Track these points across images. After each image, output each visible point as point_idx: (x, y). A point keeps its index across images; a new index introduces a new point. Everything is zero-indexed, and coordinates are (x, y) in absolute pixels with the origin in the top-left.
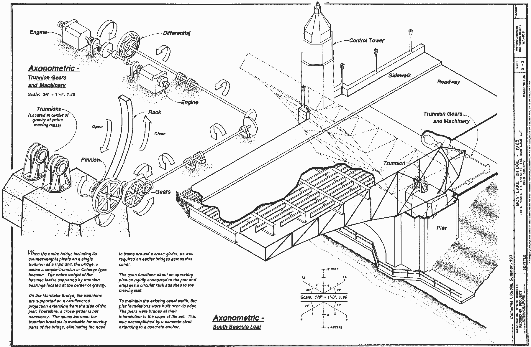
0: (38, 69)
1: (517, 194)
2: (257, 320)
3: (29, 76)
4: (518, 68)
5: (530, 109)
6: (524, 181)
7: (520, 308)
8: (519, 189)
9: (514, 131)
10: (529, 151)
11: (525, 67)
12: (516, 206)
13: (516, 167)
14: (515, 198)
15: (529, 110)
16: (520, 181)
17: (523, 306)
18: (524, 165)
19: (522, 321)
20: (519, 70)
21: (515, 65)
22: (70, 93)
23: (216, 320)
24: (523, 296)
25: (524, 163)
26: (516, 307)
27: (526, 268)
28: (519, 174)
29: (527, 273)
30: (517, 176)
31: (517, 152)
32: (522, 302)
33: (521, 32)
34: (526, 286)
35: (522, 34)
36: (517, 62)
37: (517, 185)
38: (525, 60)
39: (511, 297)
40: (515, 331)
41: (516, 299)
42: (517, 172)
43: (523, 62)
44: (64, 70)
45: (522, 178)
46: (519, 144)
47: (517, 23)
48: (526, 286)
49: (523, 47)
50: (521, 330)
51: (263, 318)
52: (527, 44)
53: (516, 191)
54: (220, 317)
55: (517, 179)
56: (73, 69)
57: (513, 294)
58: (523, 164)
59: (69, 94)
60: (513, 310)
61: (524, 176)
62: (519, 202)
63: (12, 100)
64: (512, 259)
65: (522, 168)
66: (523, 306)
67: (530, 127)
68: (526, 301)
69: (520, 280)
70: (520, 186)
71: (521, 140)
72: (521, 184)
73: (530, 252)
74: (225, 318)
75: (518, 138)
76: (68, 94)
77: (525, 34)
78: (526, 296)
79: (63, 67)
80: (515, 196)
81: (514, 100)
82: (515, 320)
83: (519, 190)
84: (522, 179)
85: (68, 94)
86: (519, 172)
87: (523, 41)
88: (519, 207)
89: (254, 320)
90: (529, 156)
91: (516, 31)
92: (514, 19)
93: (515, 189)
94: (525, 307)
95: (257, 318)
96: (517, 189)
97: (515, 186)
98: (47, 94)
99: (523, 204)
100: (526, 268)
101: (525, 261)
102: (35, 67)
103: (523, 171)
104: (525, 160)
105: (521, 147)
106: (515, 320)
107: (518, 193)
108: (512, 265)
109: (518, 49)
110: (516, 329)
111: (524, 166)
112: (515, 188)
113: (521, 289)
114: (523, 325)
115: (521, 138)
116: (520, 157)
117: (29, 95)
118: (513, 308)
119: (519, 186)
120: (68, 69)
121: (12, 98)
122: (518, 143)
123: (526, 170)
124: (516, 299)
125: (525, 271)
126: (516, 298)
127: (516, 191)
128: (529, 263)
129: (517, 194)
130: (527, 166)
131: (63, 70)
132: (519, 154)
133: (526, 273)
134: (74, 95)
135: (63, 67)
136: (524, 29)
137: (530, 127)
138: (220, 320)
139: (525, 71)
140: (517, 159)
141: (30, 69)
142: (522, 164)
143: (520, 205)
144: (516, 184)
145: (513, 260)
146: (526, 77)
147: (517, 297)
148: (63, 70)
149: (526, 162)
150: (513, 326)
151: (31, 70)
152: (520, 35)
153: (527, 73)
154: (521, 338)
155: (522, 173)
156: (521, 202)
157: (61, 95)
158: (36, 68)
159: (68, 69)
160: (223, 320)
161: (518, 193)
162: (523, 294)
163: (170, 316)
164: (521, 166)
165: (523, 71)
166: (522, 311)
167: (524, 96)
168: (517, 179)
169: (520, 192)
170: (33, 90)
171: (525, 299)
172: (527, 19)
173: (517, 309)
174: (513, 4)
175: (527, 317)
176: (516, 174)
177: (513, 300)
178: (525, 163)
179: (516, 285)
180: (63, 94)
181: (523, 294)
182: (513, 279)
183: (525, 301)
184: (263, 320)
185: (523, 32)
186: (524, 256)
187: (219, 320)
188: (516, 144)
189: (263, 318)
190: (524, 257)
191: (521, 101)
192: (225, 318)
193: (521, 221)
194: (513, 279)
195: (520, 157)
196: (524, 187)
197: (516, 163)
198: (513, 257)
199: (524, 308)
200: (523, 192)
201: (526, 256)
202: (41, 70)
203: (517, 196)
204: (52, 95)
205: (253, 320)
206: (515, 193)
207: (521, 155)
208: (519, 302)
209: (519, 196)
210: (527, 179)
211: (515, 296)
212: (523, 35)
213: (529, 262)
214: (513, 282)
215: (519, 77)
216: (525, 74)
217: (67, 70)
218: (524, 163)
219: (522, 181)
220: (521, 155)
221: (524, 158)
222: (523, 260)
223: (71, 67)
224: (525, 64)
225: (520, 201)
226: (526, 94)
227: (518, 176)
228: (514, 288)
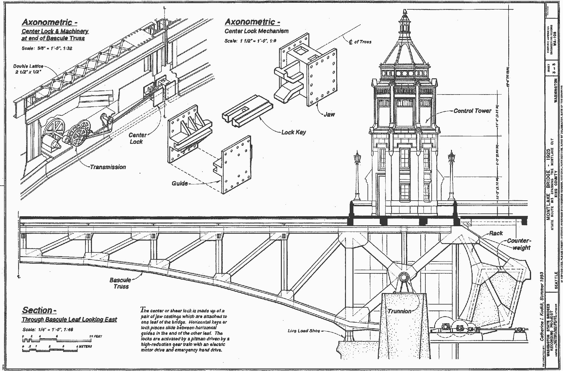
0: (32, 23)
1: (548, 207)
2: (273, 24)
3: (24, 318)
4: (549, 71)
5: (562, 116)
6: (556, 192)
7: (552, 329)
8: (550, 201)
9: (545, 116)
10: (561, 99)
11: (556, 71)
12: (547, 219)
13: (547, 214)
14: (546, 211)
15: (561, 116)
16: (552, 193)
17: (554, 327)
18: (556, 176)
19: (553, 344)
20: (551, 73)
21: (546, 68)
22: (66, 47)
23: (228, 24)
24: (554, 317)
25: (556, 173)
26: (547, 328)
27: (557, 286)
28: (550, 185)
29: (559, 292)
30: (548, 187)
31: (548, 162)
32: (553, 322)
33: (553, 32)
34: (558, 307)
35: (553, 34)
36: (548, 65)
37: (548, 197)
38: (556, 62)
39: (542, 317)
40: (546, 354)
41: (547, 320)
42: (548, 183)
43: (554, 64)
44: (61, 25)
45: (554, 189)
46: (551, 154)
47: (549, 23)
48: (558, 307)
49: (555, 48)
50: (552, 353)
51: (279, 22)
52: (559, 45)
53: (547, 203)
54: (232, 21)
55: (548, 191)
56: (70, 23)
57: (544, 315)
58: (555, 175)
59: (66, 48)
60: (544, 331)
61: (556, 187)
62: (550, 216)
63: (5, 155)
64: (543, 276)
65: (554, 179)
66: (554, 327)
67: (562, 134)
68: (557, 322)
69: (551, 299)
70: (551, 199)
71: (552, 149)
72: (552, 196)
73: (562, 270)
74: (238, 22)
75: (549, 147)
76: (65, 329)
77: (557, 34)
78: (557, 316)
79: (60, 20)
80: (546, 209)
81: (545, 125)
82: (546, 342)
83: (550, 203)
84: (554, 191)
85: (64, 47)
86: (550, 183)
87: (555, 42)
88: (550, 220)
89: (269, 24)
90: (561, 260)
91: (547, 31)
92: (545, 19)
93: (546, 202)
94: (556, 328)
95: (273, 22)
96: (548, 201)
97: (546, 198)
98: (42, 48)
99: (555, 218)
100: (557, 286)
101: (557, 279)
102: (30, 21)
103: (555, 182)
104: (557, 170)
105: (552, 157)
106: (546, 342)
107: (550, 205)
108: (543, 283)
109: (550, 51)
110: (547, 352)
111: (556, 178)
112: (546, 200)
113: (552, 308)
114: (554, 348)
115: (552, 146)
116: (552, 167)
117: (25, 311)
118: (544, 329)
119: (550, 198)
120: (65, 23)
121: (5, 198)
122: (549, 152)
123: (557, 181)
124: (547, 320)
125: (557, 290)
126: (547, 318)
127: (547, 203)
128: (560, 281)
129: (548, 207)
130: (558, 86)
131: (59, 24)
132: (550, 164)
133: (558, 292)
134: (71, 49)
135: (60, 20)
136: (555, 29)
137: (562, 134)
138: (233, 25)
139: (556, 74)
140: (547, 169)
141: (24, 23)
142: (554, 174)
143: (551, 218)
144: (547, 196)
145: (544, 277)
146: (557, 81)
147: (548, 318)
148: (59, 24)
149: (557, 172)
150: (543, 349)
151: (25, 24)
152: (551, 36)
153: (559, 76)
154: (552, 362)
155: (554, 185)
156: (552, 216)
157: (58, 331)
158: (30, 22)
159: (65, 23)
160: (235, 25)
161: (550, 205)
162: (554, 315)
163: (182, 332)
164: (552, 177)
165: (554, 74)
166: (554, 333)
167: (555, 101)
168: (548, 191)
169: (552, 205)
170: (27, 44)
171: (557, 320)
172: (559, 18)
173: (548, 330)
174: (545, 3)
175: (558, 348)
176: (547, 186)
177: (544, 321)
178: (557, 173)
179: (547, 305)
180: (60, 330)
181: (554, 315)
182: (544, 298)
183: (556, 321)
184: (279, 24)
185: (555, 33)
186: (555, 273)
187: (232, 24)
188: (548, 154)
189: (279, 22)
190: (556, 275)
191: (552, 108)
192: (238, 22)
193: (552, 237)
194: (543, 297)
195: (552, 167)
196: (556, 200)
197: (547, 174)
198: (544, 275)
199: (555, 329)
200: (555, 204)
201: (557, 273)
202: (36, 24)
203: (548, 209)
204: (49, 330)
205: (268, 24)
206: (546, 206)
207: (552, 164)
208: (550, 323)
209: (550, 209)
210: (558, 88)
211: (546, 317)
212: (555, 35)
213: (561, 280)
214: (544, 301)
215: (550, 81)
216: (557, 78)
217: (63, 24)
218: (556, 173)
219: (554, 192)
220: (552, 164)
221: (555, 167)
222: (555, 278)
223: (68, 21)
224: (556, 66)
225: (551, 215)
226: (557, 99)
227: (549, 187)
228: (545, 308)
